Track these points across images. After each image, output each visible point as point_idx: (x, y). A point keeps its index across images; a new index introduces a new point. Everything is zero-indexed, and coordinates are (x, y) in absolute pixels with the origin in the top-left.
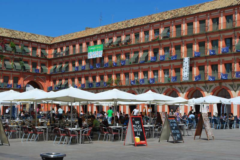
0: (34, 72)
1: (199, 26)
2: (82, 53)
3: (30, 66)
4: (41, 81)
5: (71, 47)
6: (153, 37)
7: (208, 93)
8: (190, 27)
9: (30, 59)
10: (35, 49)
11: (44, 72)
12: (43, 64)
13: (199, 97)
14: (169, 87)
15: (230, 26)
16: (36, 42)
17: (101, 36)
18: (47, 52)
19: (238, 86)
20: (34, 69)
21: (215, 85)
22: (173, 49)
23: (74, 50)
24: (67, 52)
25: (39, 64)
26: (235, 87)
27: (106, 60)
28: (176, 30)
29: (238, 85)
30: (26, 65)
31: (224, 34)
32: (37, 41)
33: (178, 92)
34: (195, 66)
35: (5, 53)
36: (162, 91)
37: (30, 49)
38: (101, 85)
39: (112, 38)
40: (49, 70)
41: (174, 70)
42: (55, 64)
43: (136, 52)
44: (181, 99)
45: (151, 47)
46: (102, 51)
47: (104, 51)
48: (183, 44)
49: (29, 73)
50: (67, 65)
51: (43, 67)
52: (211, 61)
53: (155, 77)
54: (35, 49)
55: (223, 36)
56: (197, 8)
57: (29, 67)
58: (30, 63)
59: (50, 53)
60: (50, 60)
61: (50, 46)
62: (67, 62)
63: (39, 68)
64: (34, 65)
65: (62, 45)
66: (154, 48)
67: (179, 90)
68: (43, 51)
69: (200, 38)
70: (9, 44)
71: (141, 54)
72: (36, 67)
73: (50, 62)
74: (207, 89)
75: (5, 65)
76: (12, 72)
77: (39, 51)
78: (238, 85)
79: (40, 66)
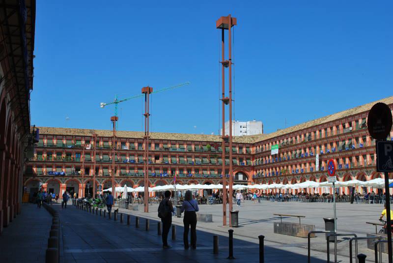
0: (241, 165)
3: (238, 161)
4: (248, 171)
5: (313, 134)
9: (237, 156)
10: (241, 148)
11: (248, 164)
12: (247, 159)
13: (165, 185)
14: (359, 171)
17: (278, 138)
18: (251, 149)
20: (241, 163)
21: (205, 180)
22: (313, 148)
23: (320, 134)
24: (262, 149)
25: (245, 159)
27: (281, 155)
30: (234, 161)
32: (243, 142)
35: (218, 153)
37: (237, 149)
38: (343, 167)
40: (252, 163)
42: (259, 158)
43: (344, 140)
44: (354, 181)
46: (278, 149)
47: (279, 149)
49: (237, 166)
51: (248, 161)
53: (365, 160)
54: (241, 148)
56: (326, 117)
57: (237, 162)
58: (238, 159)
59: (252, 150)
60: (253, 155)
61: (253, 145)
62: (262, 157)
63: (245, 162)
64: (241, 160)
65: (259, 144)
67: (366, 173)
68: (248, 149)
70: (220, 146)
71: (347, 142)
72: (242, 161)
73: (254, 157)
75: (218, 161)
76: (216, 166)
77: (244, 149)
79: (246, 160)
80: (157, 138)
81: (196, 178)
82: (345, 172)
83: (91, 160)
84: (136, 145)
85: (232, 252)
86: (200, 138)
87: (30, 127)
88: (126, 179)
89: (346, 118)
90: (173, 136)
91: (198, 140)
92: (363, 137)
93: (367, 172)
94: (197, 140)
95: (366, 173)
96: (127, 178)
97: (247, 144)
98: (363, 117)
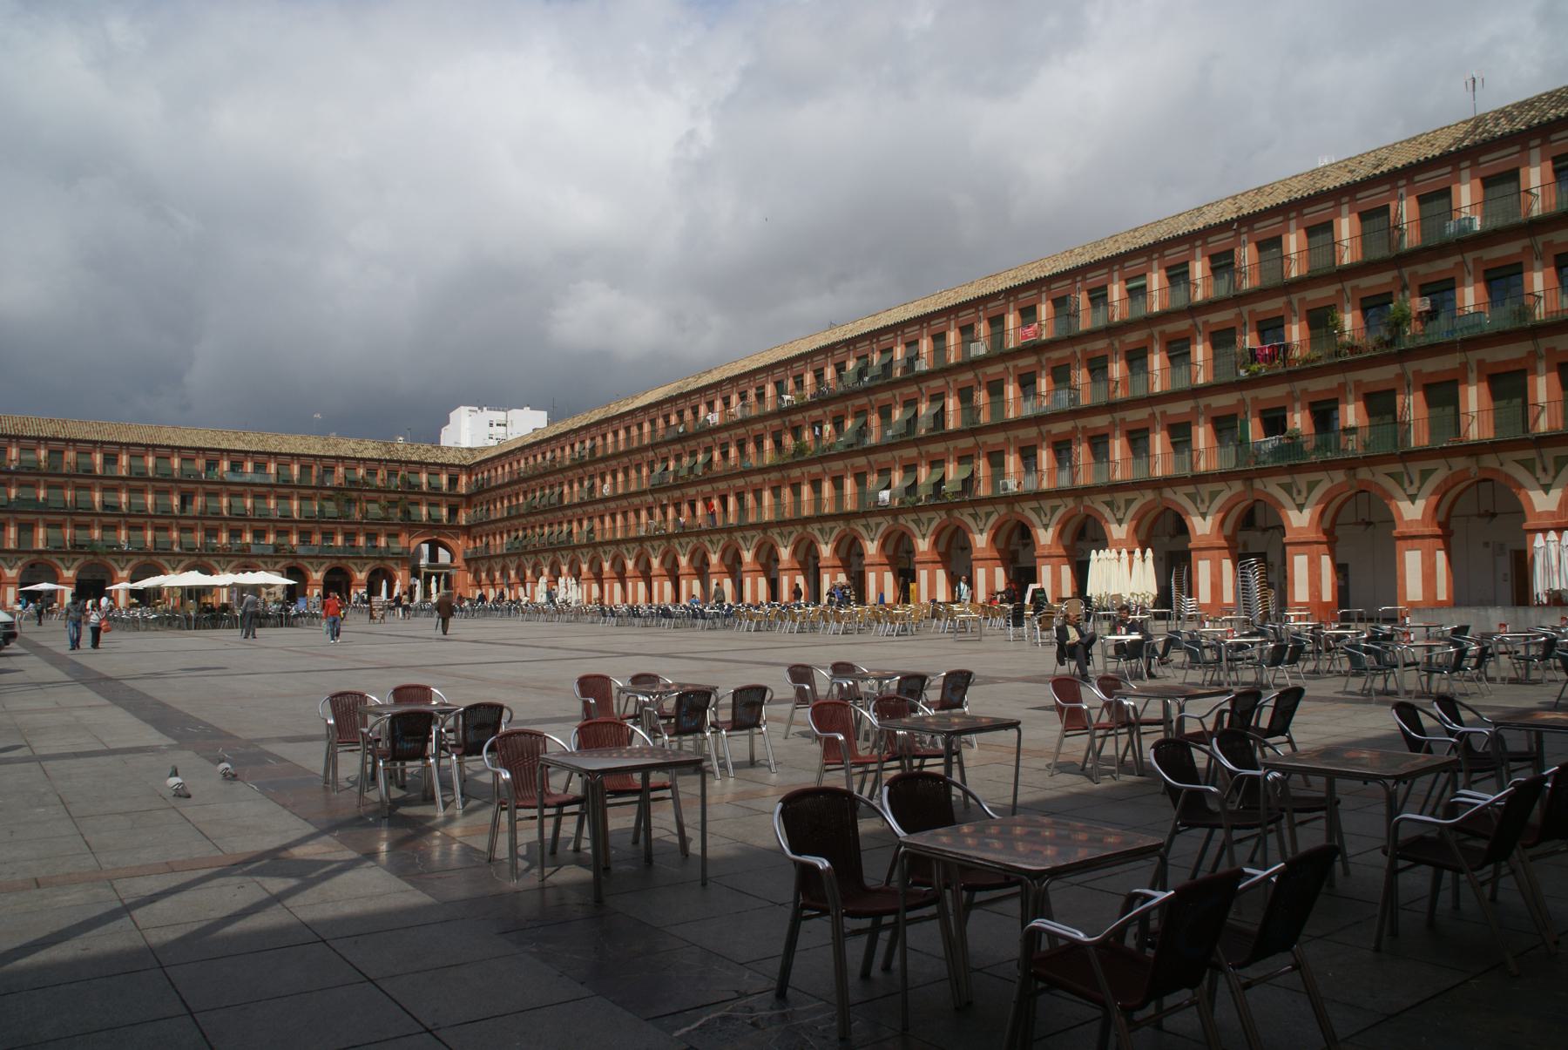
1: (1358, 232)
2: (1522, 218)
6: (1206, 286)
7: (1547, 493)
8: (1320, 239)
14: (1070, 503)
15: (1222, 289)
16: (435, 464)
19: (1560, 463)
26: (1299, 492)
28: (1485, 196)
29: (1556, 458)
31: (1355, 282)
33: (1521, 487)
34: (1473, 376)
36: (1422, 484)
39: (890, 350)
41: (1420, 395)
45: (1471, 266)
48: (1042, 367)
50: (861, 421)
52: (1489, 360)
55: (1084, 352)
66: (1261, 318)
69: (1172, 328)
74: (1411, 483)
78: (1556, 458)
80: (189, 444)
81: (303, 557)
82: (943, 514)
83: (119, 507)
84: (98, 458)
85: (68, 939)
86: (318, 447)
87: (286, 433)
88: (90, 557)
89: (671, 400)
90: (238, 439)
91: (312, 452)
92: (990, 455)
93: (867, 527)
94: (306, 452)
95: (864, 533)
96: (95, 554)
97: (453, 465)
98: (709, 398)
